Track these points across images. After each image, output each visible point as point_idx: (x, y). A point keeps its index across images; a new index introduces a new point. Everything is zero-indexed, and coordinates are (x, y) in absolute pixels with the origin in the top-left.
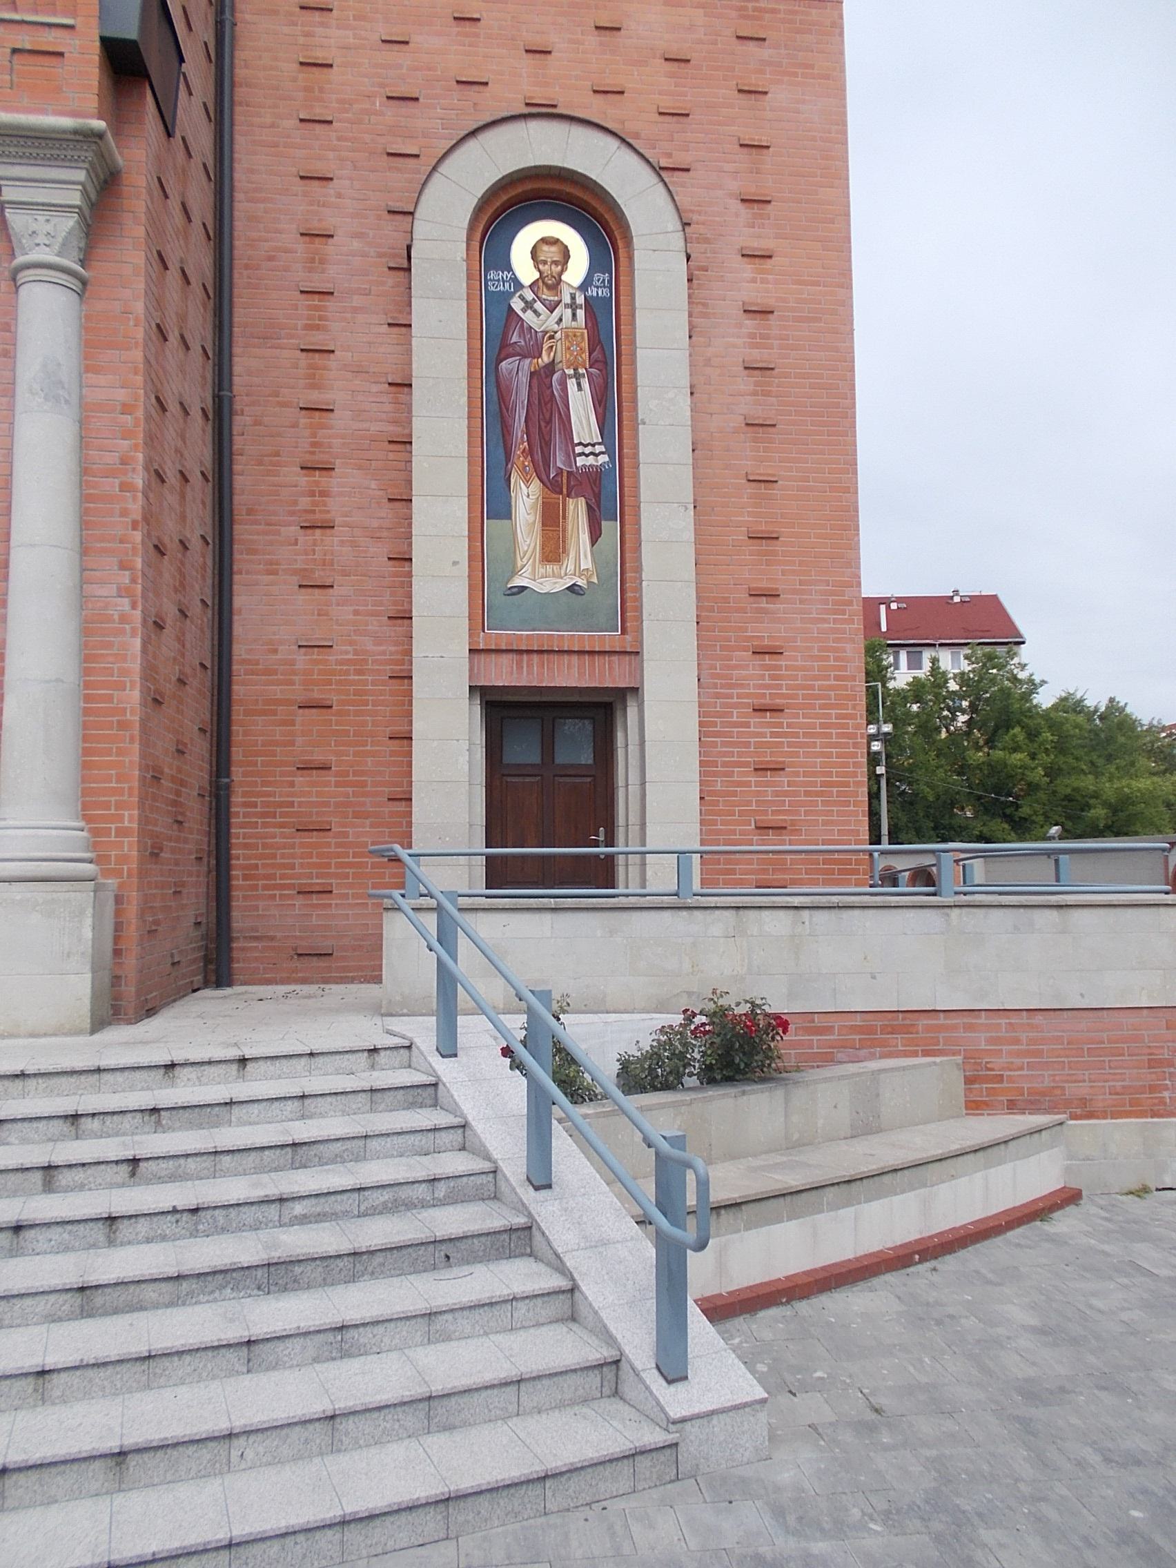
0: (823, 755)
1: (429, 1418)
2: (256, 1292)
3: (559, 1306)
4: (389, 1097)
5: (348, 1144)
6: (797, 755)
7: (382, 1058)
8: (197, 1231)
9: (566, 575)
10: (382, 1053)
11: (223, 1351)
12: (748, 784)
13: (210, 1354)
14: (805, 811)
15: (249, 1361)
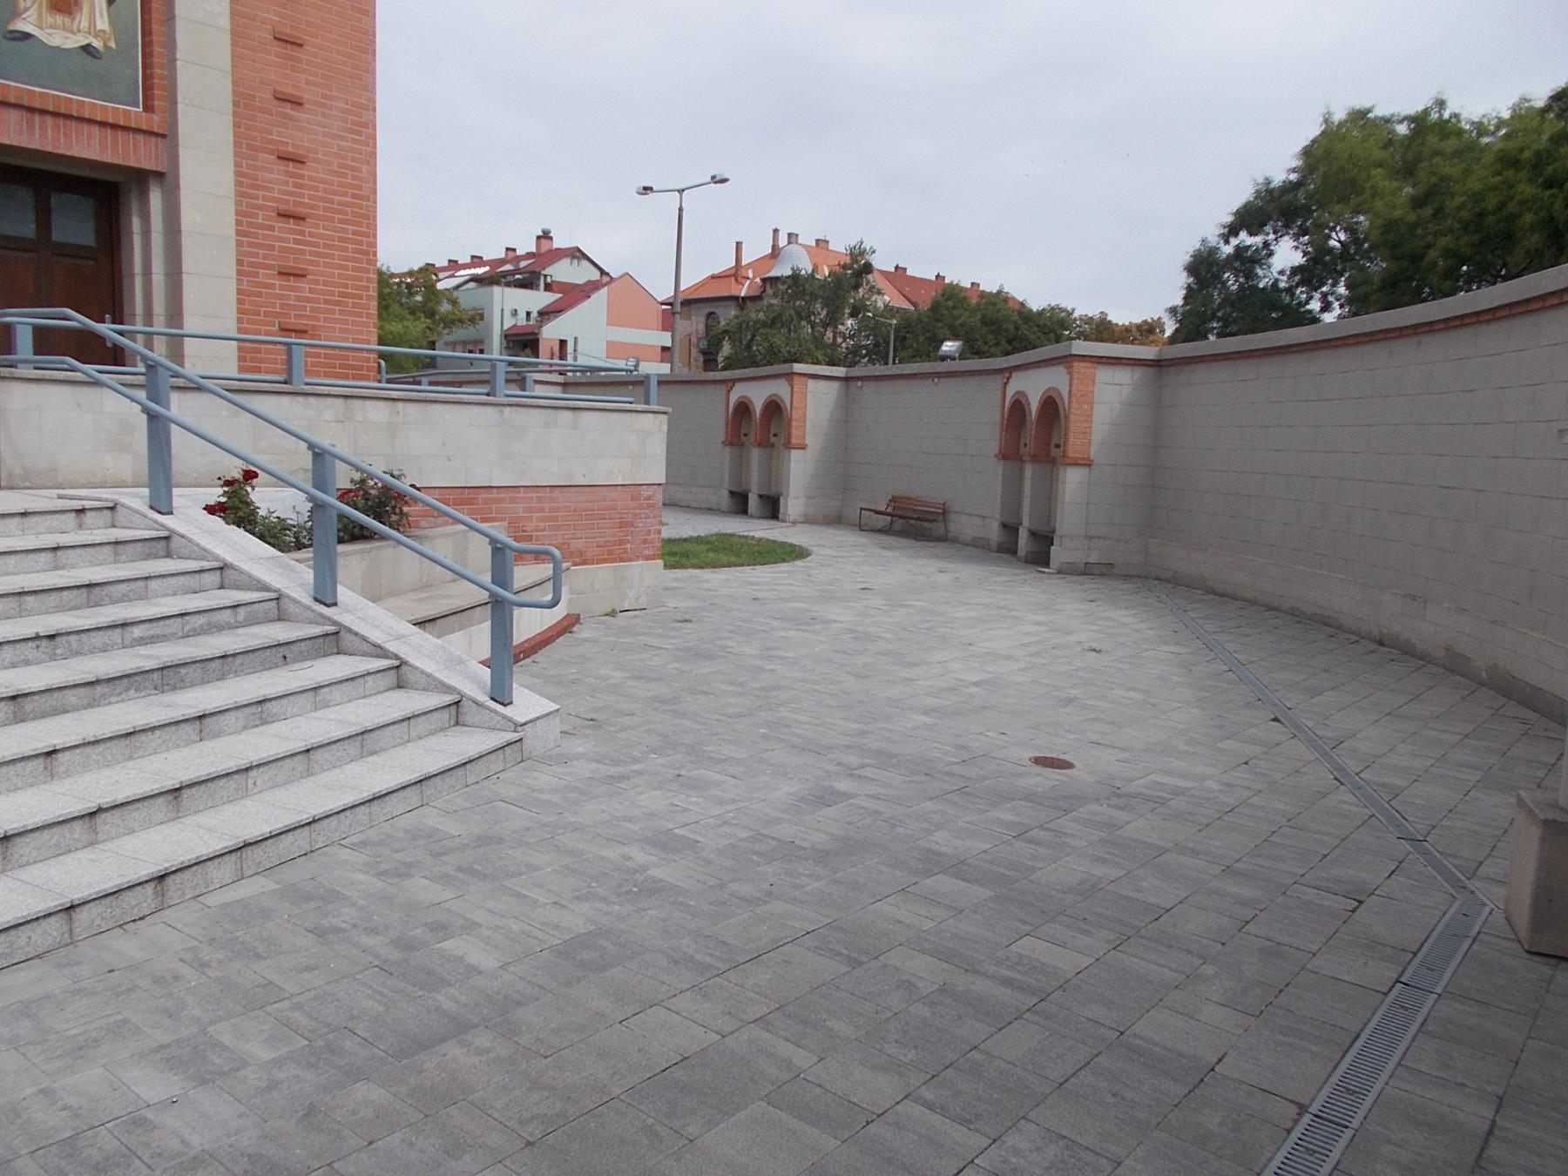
0: (340, 267)
1: (362, 747)
2: (154, 692)
3: (391, 678)
4: (129, 548)
5: (133, 585)
6: (317, 264)
7: (89, 518)
8: (56, 654)
9: (79, 31)
10: (89, 514)
11: (183, 725)
12: (272, 286)
13: (174, 728)
14: (325, 318)
15: (201, 731)
